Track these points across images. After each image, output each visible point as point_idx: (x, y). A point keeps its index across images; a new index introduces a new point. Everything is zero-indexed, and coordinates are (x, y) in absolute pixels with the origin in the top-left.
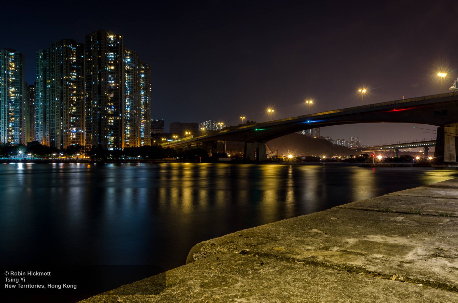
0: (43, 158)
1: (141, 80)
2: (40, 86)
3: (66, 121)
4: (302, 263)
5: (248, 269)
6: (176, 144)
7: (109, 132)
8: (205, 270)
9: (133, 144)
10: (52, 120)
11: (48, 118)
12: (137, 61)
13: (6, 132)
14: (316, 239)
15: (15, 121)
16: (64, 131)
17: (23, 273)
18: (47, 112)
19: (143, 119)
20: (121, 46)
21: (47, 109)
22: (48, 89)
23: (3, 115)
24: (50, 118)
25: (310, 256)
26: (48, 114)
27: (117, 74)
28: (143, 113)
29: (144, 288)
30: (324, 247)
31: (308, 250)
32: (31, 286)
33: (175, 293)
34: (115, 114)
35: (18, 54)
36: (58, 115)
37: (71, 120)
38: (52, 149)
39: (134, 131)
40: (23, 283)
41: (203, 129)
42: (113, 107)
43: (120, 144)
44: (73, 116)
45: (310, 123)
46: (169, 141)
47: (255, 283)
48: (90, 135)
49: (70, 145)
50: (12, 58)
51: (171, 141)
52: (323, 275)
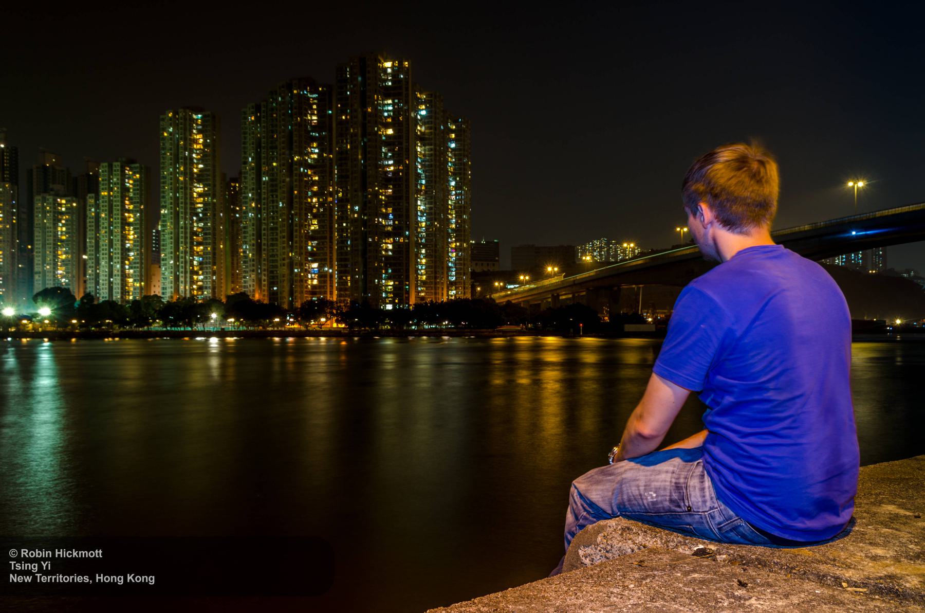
0: (256, 328)
1: (450, 155)
2: (250, 181)
4: (861, 590)
6: (525, 295)
7: (384, 271)
8: (611, 589)
9: (433, 296)
10: (271, 248)
11: (264, 245)
12: (442, 114)
13: (188, 275)
14: (894, 531)
15: (205, 252)
16: (296, 270)
17: (47, 552)
18: (263, 232)
19: (454, 239)
20: (407, 83)
21: (264, 227)
22: (264, 184)
25: (882, 575)
27: (400, 144)
28: (454, 226)
30: (921, 553)
31: (875, 558)
32: (62, 578)
34: (397, 231)
35: (208, 116)
36: (284, 237)
37: (309, 248)
38: (272, 309)
39: (435, 267)
40: (46, 573)
41: (588, 258)
42: (391, 216)
43: (405, 296)
44: (312, 239)
45: (856, 236)
46: (509, 287)
49: (307, 299)
50: (197, 124)
51: (515, 288)
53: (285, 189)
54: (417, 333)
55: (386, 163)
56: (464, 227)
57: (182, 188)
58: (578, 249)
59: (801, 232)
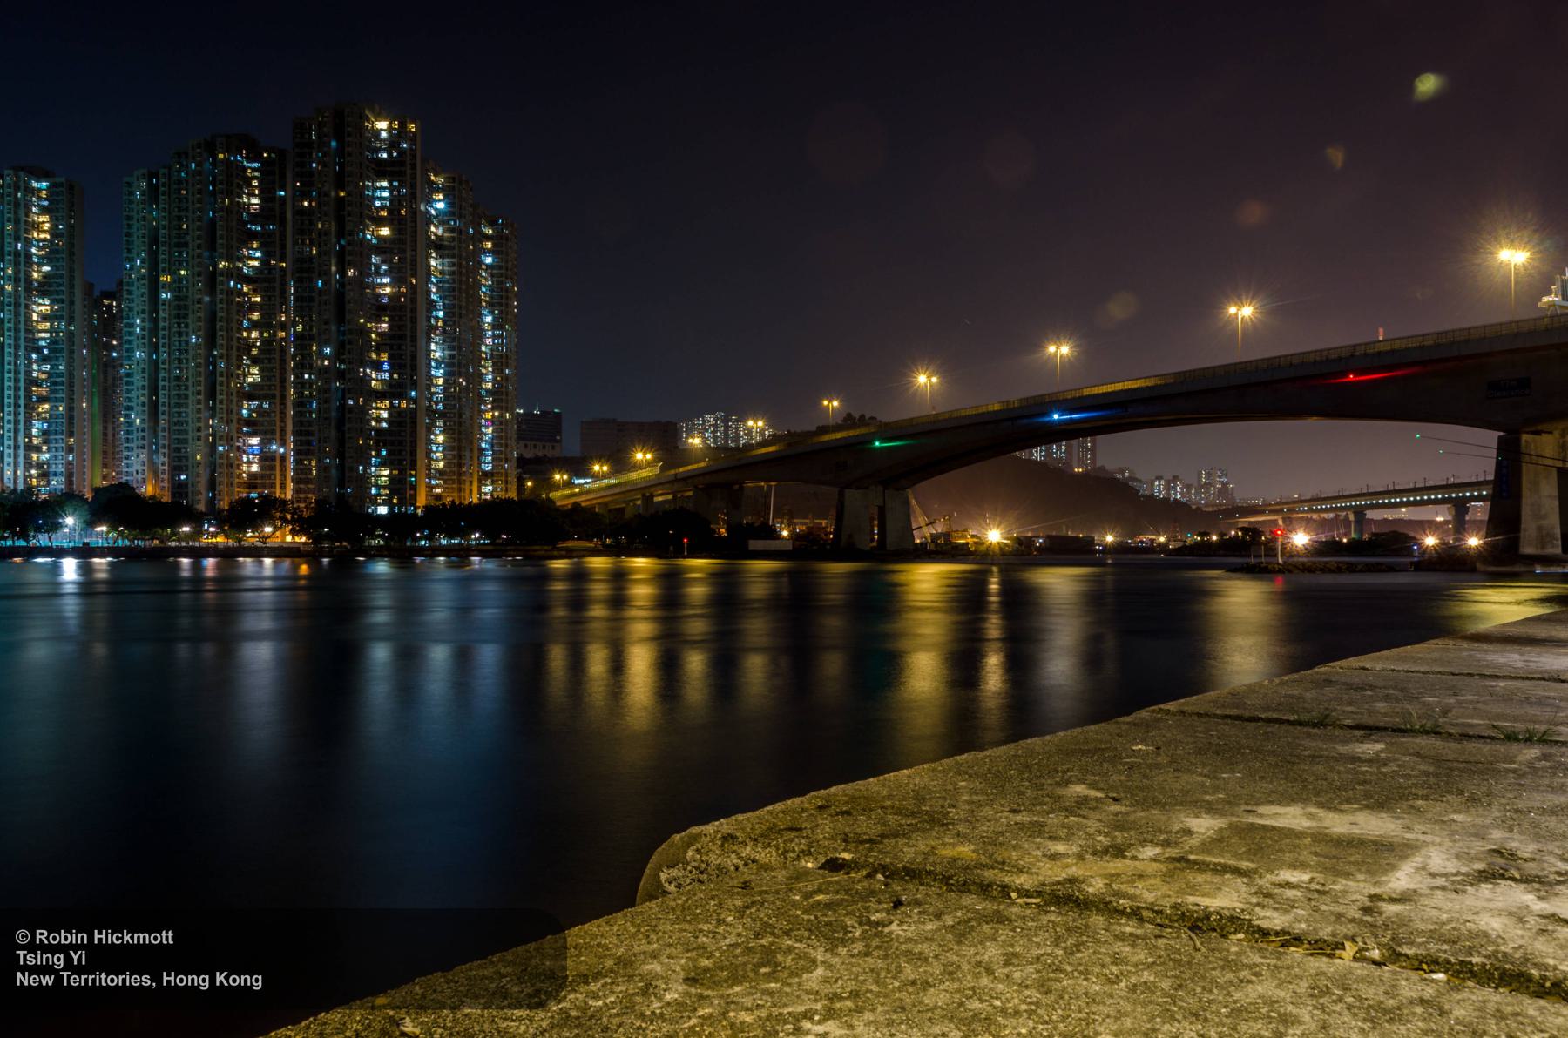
0: (148, 543)
1: (484, 274)
2: (138, 296)
3: (225, 415)
4: (1033, 900)
5: (849, 923)
6: (602, 494)
7: (373, 453)
9: (456, 494)
10: (177, 410)
11: (164, 404)
12: (470, 209)
13: (21, 452)
14: (1081, 820)
16: (220, 448)
17: (79, 935)
18: (161, 383)
19: (489, 406)
20: (414, 156)
21: (162, 374)
22: (163, 304)
23: (12, 392)
24: (172, 402)
26: (166, 392)
27: (402, 252)
28: (490, 385)
29: (493, 985)
30: (1110, 846)
31: (1054, 857)
32: (106, 979)
33: (600, 1003)
34: (393, 391)
35: (61, 185)
36: (199, 393)
37: (244, 412)
38: (177, 510)
39: (460, 449)
40: (79, 970)
41: (696, 441)
42: (386, 367)
43: (409, 492)
44: (250, 397)
45: (1060, 422)
46: (577, 481)
47: (872, 970)
48: (310, 461)
49: (241, 495)
50: (40, 198)
51: (586, 483)
52: (1106, 941)
53: (201, 315)
54: (430, 552)
55: (379, 280)
56: (507, 387)
57: (9, 305)
58: (682, 427)
59: (989, 413)
